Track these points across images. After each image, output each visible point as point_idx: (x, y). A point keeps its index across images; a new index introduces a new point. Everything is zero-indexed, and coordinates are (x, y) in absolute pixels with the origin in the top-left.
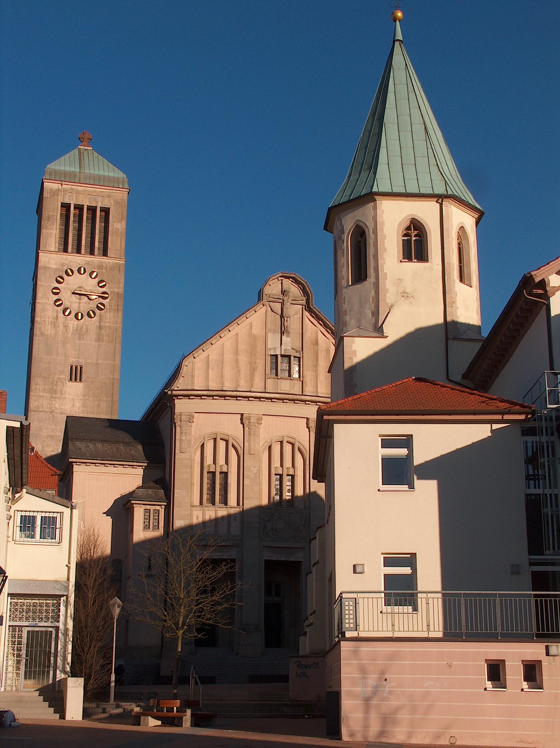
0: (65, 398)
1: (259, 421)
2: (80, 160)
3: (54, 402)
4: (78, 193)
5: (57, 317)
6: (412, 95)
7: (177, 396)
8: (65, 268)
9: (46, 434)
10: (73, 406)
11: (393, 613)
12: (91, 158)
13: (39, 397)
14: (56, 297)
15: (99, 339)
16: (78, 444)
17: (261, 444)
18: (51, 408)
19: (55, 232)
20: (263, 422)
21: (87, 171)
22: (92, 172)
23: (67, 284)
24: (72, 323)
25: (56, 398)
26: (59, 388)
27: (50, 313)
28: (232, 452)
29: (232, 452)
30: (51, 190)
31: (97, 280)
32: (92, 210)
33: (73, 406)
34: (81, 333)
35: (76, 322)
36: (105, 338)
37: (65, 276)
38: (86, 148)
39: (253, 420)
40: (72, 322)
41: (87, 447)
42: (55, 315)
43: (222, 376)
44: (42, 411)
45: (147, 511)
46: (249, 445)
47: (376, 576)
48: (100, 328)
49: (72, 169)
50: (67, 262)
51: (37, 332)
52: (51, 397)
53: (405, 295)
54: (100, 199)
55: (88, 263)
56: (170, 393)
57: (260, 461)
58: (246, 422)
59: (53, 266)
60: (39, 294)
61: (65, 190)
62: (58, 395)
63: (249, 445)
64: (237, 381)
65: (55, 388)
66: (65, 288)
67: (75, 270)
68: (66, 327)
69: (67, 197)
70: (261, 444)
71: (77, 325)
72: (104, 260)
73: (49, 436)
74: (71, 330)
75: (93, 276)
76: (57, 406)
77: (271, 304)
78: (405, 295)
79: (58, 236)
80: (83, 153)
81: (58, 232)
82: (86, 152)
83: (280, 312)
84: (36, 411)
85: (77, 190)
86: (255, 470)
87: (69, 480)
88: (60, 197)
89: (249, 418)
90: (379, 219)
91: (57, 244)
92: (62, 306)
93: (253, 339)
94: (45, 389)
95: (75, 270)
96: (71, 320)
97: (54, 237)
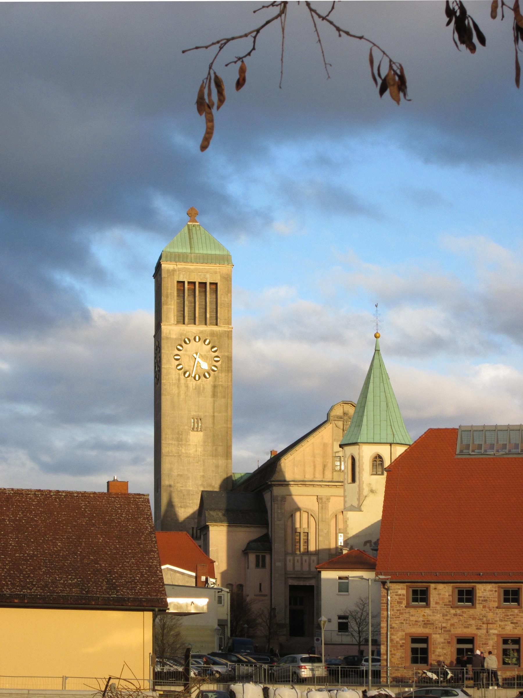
0: (190, 444)
1: (328, 499)
2: (190, 239)
3: (180, 448)
4: (191, 271)
5: (179, 380)
6: (382, 384)
7: (275, 485)
8: (183, 337)
9: (176, 474)
10: (196, 451)
11: (342, 635)
12: (199, 232)
13: (169, 444)
14: (177, 363)
15: (214, 395)
16: (212, 513)
17: (330, 514)
18: (178, 453)
19: (173, 307)
20: (331, 500)
21: (197, 252)
22: (201, 252)
23: (186, 351)
24: (192, 383)
25: (181, 445)
26: (184, 436)
27: (173, 376)
28: (312, 520)
29: (312, 520)
30: (168, 270)
31: (210, 346)
32: (203, 285)
33: (196, 451)
34: (199, 391)
35: (194, 382)
36: (219, 394)
37: (184, 344)
38: (194, 223)
39: (324, 500)
40: (191, 383)
41: (217, 514)
42: (177, 377)
43: (304, 472)
44: (171, 456)
45: (257, 557)
46: (322, 515)
47: (334, 626)
48: (215, 387)
49: (184, 251)
50: (185, 332)
51: (164, 392)
52: (179, 444)
53: (372, 491)
54: (208, 276)
55: (202, 332)
56: (270, 483)
57: (329, 525)
58: (320, 501)
59: (174, 336)
60: (164, 361)
61: (179, 270)
62: (184, 442)
63: (322, 515)
64: (314, 474)
65: (181, 436)
66: (184, 355)
67: (192, 339)
68: (187, 387)
69: (181, 276)
70: (330, 514)
71: (196, 384)
72: (215, 328)
73: (178, 475)
74: (191, 389)
75: (206, 343)
76: (183, 451)
77: (336, 422)
78: (372, 491)
79: (176, 310)
80: (192, 230)
81: (175, 306)
82: (194, 228)
83: (342, 427)
84: (166, 456)
85: (189, 269)
86: (325, 531)
87: (206, 534)
88: (175, 277)
89: (321, 499)
90: (361, 454)
91: (176, 317)
92: (183, 370)
93: (325, 445)
94: (173, 438)
95: (192, 339)
96: (191, 380)
97: (173, 312)
